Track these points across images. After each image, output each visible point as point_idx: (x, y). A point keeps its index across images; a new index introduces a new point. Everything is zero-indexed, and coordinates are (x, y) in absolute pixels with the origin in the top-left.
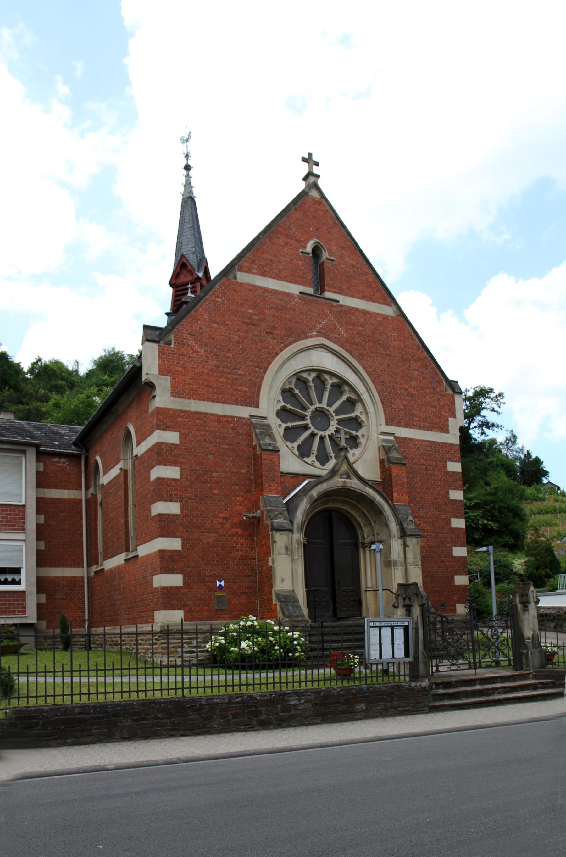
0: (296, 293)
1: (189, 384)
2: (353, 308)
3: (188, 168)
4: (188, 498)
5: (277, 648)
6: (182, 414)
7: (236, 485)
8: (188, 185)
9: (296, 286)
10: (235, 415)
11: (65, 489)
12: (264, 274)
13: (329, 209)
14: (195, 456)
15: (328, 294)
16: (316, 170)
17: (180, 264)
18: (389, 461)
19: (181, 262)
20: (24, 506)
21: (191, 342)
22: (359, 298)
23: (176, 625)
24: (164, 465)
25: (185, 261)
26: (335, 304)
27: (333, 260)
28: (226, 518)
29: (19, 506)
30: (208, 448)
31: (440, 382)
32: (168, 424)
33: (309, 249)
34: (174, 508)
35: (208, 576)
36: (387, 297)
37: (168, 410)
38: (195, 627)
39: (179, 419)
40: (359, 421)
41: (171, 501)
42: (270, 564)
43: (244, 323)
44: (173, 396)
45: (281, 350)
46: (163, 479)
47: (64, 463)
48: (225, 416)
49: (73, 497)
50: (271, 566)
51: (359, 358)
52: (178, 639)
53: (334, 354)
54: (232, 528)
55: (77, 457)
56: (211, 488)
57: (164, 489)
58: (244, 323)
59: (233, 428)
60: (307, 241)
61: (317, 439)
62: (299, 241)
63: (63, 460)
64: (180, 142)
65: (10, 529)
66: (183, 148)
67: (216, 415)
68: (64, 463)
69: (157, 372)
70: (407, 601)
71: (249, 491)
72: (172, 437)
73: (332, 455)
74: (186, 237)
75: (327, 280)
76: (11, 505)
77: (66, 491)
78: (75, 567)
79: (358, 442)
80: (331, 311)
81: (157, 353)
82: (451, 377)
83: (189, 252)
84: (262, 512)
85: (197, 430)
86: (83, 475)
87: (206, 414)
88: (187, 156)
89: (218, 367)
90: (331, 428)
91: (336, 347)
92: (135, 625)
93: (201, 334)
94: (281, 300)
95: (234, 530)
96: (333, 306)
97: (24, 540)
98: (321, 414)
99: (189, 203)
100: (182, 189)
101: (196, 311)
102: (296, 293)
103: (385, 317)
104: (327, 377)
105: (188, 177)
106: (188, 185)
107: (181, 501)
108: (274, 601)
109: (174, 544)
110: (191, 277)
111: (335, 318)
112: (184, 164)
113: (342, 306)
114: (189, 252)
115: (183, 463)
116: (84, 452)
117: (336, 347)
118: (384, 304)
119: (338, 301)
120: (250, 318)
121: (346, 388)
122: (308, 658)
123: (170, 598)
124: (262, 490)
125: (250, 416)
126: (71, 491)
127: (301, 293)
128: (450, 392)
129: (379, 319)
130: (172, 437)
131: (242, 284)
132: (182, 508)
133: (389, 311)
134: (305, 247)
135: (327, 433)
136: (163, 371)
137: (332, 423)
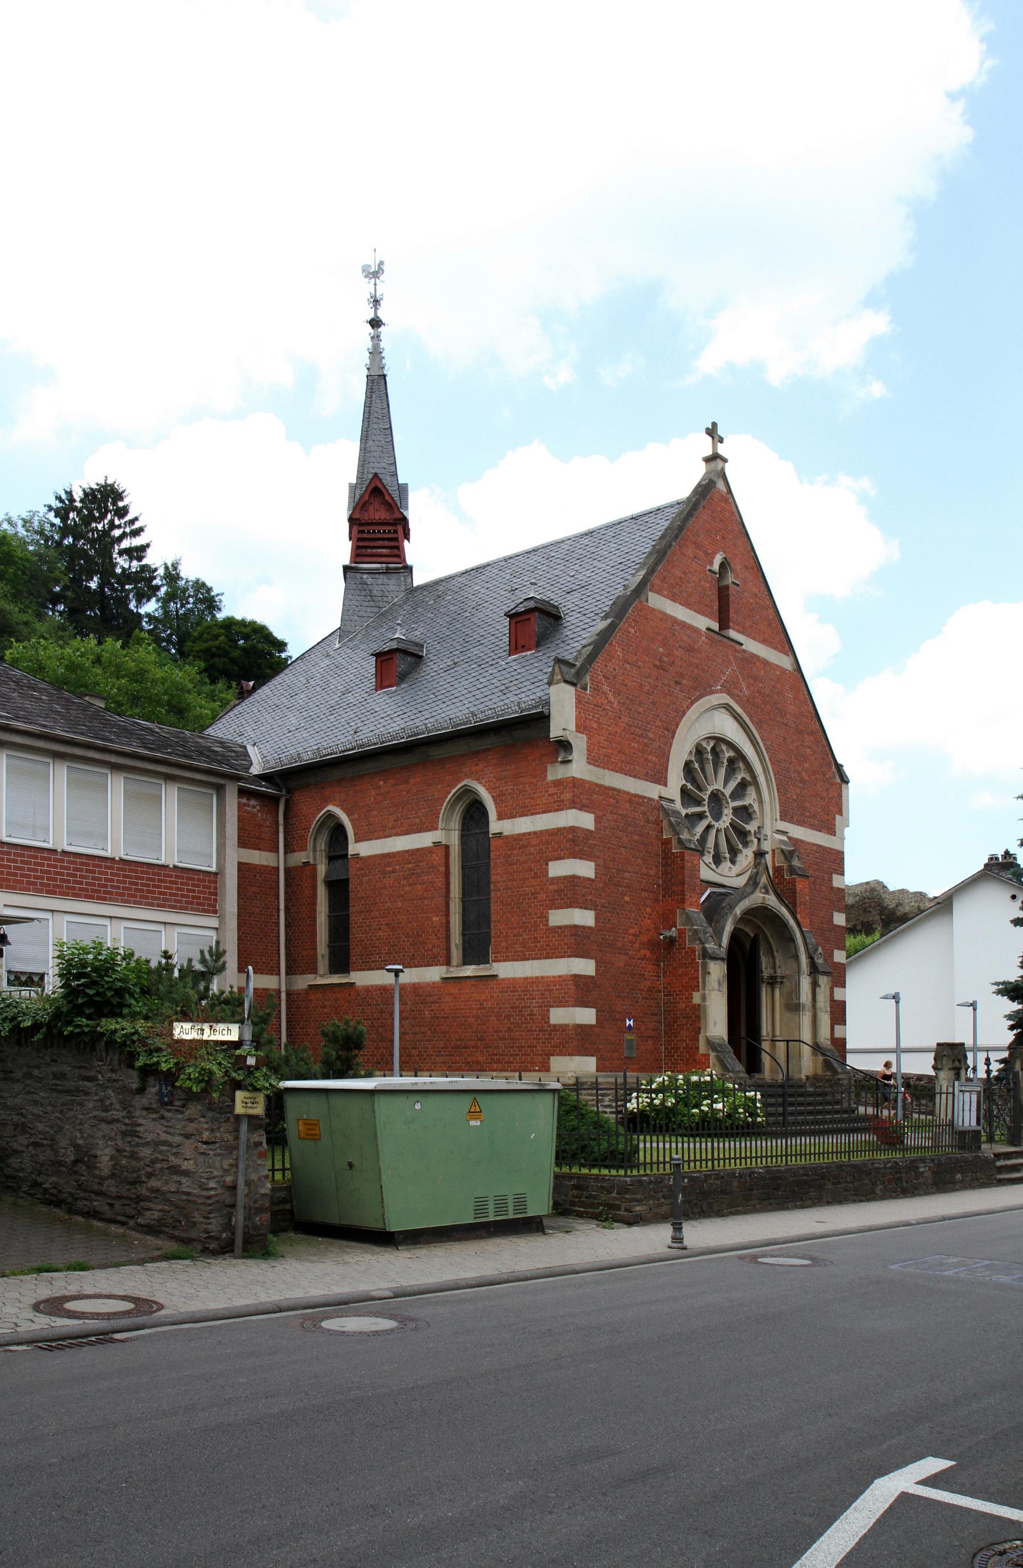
0: (703, 628)
1: (603, 748)
2: (755, 655)
3: (375, 323)
4: (602, 906)
5: (741, 1110)
6: (597, 789)
7: (645, 891)
8: (376, 353)
9: (703, 618)
10: (646, 795)
11: (255, 849)
12: (673, 598)
13: (734, 509)
14: (609, 848)
15: (733, 634)
16: (721, 450)
17: (370, 489)
18: (792, 870)
19: (373, 486)
20: (216, 874)
21: (606, 688)
22: (760, 642)
23: (591, 1076)
24: (581, 858)
25: (380, 485)
26: (738, 647)
27: (737, 585)
28: (635, 935)
29: (210, 873)
30: (620, 839)
31: (829, 765)
32: (584, 801)
33: (716, 567)
34: (585, 918)
35: (619, 1013)
36: (786, 646)
37: (583, 781)
38: (614, 1080)
39: (595, 796)
40: (750, 811)
41: (586, 908)
42: (696, 998)
43: (655, 665)
44: (589, 763)
45: (688, 708)
46: (579, 877)
47: (254, 807)
48: (636, 796)
49: (265, 864)
50: (699, 1005)
51: (759, 726)
52: (591, 1095)
53: (735, 718)
54: (641, 948)
55: (275, 800)
56: (623, 894)
57: (571, 892)
58: (655, 665)
59: (644, 814)
60: (714, 554)
61: (713, 833)
62: (706, 553)
63: (253, 802)
64: (360, 276)
65: (198, 910)
66: (367, 287)
67: (628, 793)
68: (254, 807)
69: (574, 729)
70: (957, 1063)
71: (657, 900)
72: (586, 820)
73: (727, 855)
74: (377, 443)
75: (732, 615)
76: (200, 871)
77: (257, 852)
78: (267, 974)
79: (748, 839)
80: (734, 656)
81: (574, 701)
82: (839, 762)
83: (383, 471)
84: (681, 932)
85: (611, 813)
86: (281, 829)
87: (618, 791)
88: (376, 302)
89: (630, 726)
90: (724, 818)
91: (739, 710)
92: (517, 1074)
93: (614, 677)
94: (690, 637)
95: (643, 952)
96: (736, 651)
97: (217, 929)
98: (716, 798)
99: (377, 384)
100: (366, 359)
101: (610, 644)
102: (703, 628)
103: (783, 671)
104: (724, 747)
105: (376, 338)
106: (376, 353)
107: (595, 910)
108: (703, 1048)
109: (586, 967)
110: (388, 514)
111: (738, 667)
112: (371, 315)
113: (744, 651)
114: (383, 471)
115: (598, 857)
116: (284, 792)
117: (739, 710)
118: (781, 652)
119: (741, 644)
120: (660, 660)
121: (741, 765)
122: (768, 1124)
123: (579, 1040)
124: (683, 901)
125: (660, 797)
126: (264, 853)
127: (708, 629)
128: (838, 780)
129: (778, 673)
130: (586, 820)
131: (653, 609)
132: (597, 919)
133: (786, 663)
134: (712, 563)
135: (716, 825)
136: (581, 728)
137: (726, 811)
